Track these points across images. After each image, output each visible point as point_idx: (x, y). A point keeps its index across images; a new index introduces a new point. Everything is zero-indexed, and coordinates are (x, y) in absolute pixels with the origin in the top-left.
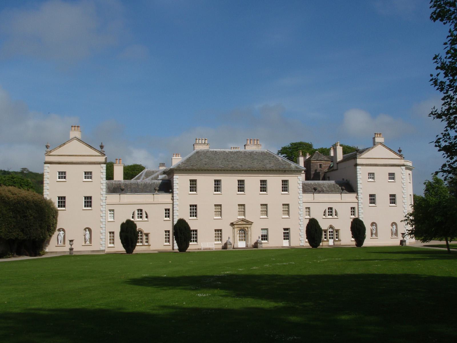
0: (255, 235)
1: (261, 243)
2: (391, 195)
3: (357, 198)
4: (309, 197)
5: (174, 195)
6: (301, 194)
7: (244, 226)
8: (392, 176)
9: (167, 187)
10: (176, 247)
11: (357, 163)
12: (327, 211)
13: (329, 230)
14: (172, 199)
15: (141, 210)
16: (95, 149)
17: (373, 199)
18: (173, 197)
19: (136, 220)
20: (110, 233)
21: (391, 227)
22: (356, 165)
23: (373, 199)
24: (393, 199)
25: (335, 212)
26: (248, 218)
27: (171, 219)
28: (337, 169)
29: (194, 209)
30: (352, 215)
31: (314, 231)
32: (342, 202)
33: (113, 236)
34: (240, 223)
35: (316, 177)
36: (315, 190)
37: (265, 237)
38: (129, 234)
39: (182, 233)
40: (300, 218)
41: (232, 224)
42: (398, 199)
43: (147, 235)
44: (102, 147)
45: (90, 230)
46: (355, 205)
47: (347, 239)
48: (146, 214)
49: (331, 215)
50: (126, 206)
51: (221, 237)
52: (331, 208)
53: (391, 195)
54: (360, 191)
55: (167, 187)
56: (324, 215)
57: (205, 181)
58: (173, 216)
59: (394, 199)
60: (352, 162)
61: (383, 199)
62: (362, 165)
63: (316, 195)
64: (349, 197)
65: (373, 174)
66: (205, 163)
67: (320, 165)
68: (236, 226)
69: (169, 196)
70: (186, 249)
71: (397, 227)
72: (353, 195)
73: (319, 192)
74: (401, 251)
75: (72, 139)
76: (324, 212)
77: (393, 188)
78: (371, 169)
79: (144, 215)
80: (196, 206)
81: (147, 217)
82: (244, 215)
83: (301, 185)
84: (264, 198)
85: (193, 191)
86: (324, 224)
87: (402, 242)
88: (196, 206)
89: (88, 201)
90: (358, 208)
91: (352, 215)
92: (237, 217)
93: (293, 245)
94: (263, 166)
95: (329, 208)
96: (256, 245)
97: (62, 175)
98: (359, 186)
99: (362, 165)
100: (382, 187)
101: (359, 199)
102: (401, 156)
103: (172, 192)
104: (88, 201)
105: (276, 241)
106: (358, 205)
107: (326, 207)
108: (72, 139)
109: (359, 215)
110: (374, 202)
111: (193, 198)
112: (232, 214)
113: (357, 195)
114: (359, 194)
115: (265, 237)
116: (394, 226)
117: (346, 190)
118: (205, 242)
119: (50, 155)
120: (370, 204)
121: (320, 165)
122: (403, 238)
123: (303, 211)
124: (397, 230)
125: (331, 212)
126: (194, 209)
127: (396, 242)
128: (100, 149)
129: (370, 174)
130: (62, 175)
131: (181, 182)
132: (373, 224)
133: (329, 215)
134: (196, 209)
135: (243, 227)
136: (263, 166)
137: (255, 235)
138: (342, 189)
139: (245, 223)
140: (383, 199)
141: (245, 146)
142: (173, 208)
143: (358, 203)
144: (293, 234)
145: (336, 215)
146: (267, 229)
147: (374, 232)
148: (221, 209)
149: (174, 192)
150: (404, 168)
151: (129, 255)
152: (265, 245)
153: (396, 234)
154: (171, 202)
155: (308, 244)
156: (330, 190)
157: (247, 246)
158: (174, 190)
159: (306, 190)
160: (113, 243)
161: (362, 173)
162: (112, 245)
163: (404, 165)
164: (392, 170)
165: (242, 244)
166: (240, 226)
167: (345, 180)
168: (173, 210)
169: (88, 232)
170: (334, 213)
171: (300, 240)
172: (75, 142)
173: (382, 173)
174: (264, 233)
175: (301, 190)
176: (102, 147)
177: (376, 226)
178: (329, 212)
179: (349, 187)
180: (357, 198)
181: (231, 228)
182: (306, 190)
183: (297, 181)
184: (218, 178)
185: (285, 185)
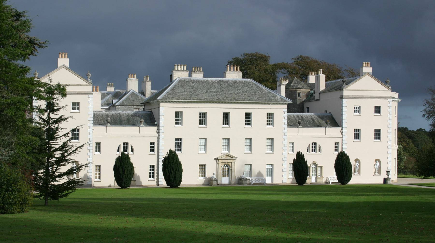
3: (342, 133)
4: (101, 129)
5: (160, 128)
6: (92, 127)
9: (151, 119)
10: (163, 182)
11: (344, 94)
12: (311, 146)
13: (312, 167)
14: (157, 132)
15: (127, 144)
17: (357, 134)
18: (158, 129)
21: (375, 163)
22: (342, 97)
23: (357, 134)
24: (378, 134)
25: (322, 147)
26: (231, 153)
28: (319, 100)
30: (335, 151)
32: (326, 136)
34: (224, 158)
35: (301, 108)
38: (123, 169)
39: (172, 167)
40: (89, 154)
41: (217, 159)
43: (321, 167)
45: (379, 161)
46: (339, 141)
47: (330, 176)
48: (132, 148)
49: (315, 151)
50: (114, 137)
51: (205, 173)
54: (345, 125)
55: (151, 119)
58: (158, 150)
59: (379, 135)
61: (367, 134)
62: (348, 97)
63: (301, 129)
64: (334, 131)
65: (78, 104)
66: (191, 93)
69: (155, 128)
70: (179, 184)
71: (380, 164)
74: (385, 188)
76: (119, 148)
77: (378, 122)
78: (357, 102)
80: (181, 139)
82: (228, 150)
83: (286, 118)
85: (178, 124)
87: (385, 180)
88: (181, 139)
90: (342, 142)
91: (335, 151)
92: (222, 152)
93: (275, 182)
94: (249, 98)
95: (124, 144)
97: (357, 109)
99: (348, 97)
100: (367, 122)
101: (344, 134)
103: (158, 125)
106: (342, 140)
107: (309, 142)
110: (358, 137)
113: (342, 129)
114: (344, 129)
117: (330, 124)
118: (190, 178)
119: (347, 90)
120: (354, 139)
122: (388, 175)
123: (288, 147)
124: (380, 168)
125: (315, 147)
126: (179, 141)
127: (379, 180)
129: (356, 108)
132: (356, 160)
133: (312, 151)
134: (181, 143)
136: (249, 98)
140: (367, 134)
142: (158, 141)
143: (342, 138)
146: (272, 165)
147: (357, 169)
149: (160, 125)
150: (390, 100)
153: (379, 172)
154: (157, 135)
155: (116, 184)
156: (314, 124)
157: (230, 182)
158: (160, 122)
159: (291, 123)
160: (99, 178)
161: (348, 105)
162: (98, 180)
165: (225, 181)
167: (328, 112)
168: (158, 144)
171: (285, 176)
172: (63, 70)
173: (368, 107)
175: (286, 123)
177: (359, 163)
178: (312, 147)
179: (333, 120)
180: (342, 133)
182: (291, 123)
183: (281, 113)
185: (203, 117)
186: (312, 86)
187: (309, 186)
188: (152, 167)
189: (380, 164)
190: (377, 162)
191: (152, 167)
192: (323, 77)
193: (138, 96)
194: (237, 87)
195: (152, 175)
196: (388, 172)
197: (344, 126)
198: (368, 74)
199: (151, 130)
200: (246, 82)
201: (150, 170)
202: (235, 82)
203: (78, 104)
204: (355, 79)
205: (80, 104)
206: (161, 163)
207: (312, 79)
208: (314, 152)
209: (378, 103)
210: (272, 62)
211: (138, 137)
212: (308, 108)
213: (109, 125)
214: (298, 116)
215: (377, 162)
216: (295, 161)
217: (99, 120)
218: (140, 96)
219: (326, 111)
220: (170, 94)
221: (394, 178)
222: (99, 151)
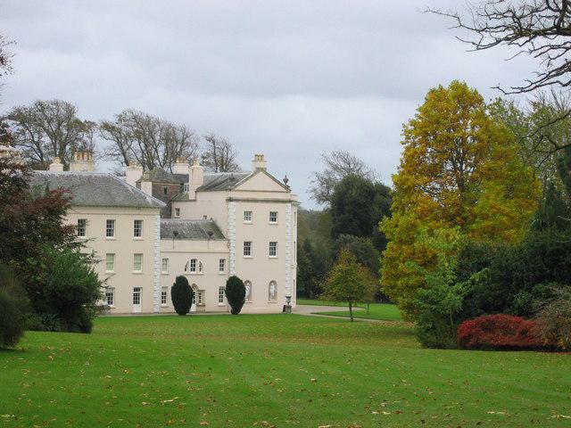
3: (229, 246)
17: (247, 248)
23: (247, 248)
61: (261, 248)
63: (177, 242)
67: (165, 190)
72: (224, 243)
73: (180, 238)
79: (197, 267)
107: (189, 258)
121: (165, 190)
124: (275, 292)
128: (283, 183)
144: (143, 296)
163: (290, 201)
167: (208, 218)
171: (156, 301)
176: (286, 181)
183: (152, 223)
189: (276, 288)
208: (193, 272)
212: (178, 210)
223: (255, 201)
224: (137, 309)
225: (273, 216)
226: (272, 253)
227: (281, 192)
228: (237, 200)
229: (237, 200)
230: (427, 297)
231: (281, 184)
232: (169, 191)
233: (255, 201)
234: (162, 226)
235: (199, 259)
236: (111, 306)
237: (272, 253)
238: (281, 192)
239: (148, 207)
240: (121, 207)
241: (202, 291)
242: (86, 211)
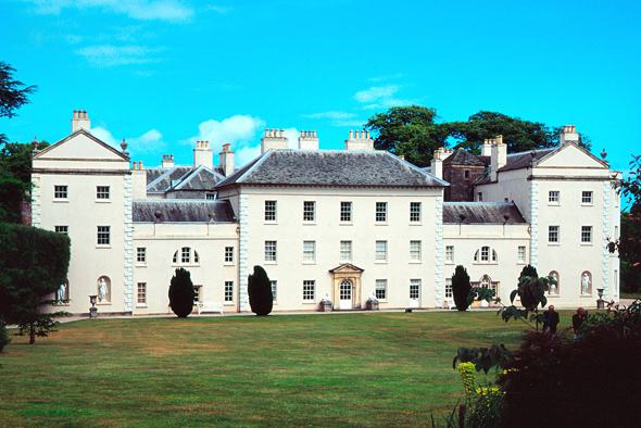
0: (365, 291)
1: (377, 304)
2: (551, 228)
3: (529, 232)
4: (146, 229)
7: (350, 275)
8: (587, 196)
9: (227, 213)
10: (246, 307)
12: (480, 252)
16: (595, 158)
17: (553, 234)
19: (186, 266)
20: (139, 284)
23: (553, 234)
27: (236, 264)
28: (496, 182)
29: (271, 248)
31: (461, 287)
33: (144, 290)
36: (467, 218)
37: (381, 293)
38: (183, 292)
41: (331, 272)
42: (561, 234)
44: (124, 146)
45: (107, 279)
46: (526, 244)
48: (196, 255)
50: (166, 241)
52: (487, 248)
53: (551, 228)
54: (534, 221)
55: (227, 213)
56: (175, 260)
57: (290, 204)
60: (524, 173)
61: (570, 233)
62: (43, 171)
63: (464, 227)
64: (518, 230)
65: (107, 188)
67: (467, 172)
68: (337, 275)
71: (590, 279)
72: (524, 227)
75: (77, 133)
77: (587, 216)
78: (61, 180)
79: (491, 256)
81: (196, 260)
82: (350, 258)
84: (381, 231)
86: (475, 276)
87: (600, 302)
89: (104, 235)
95: (483, 249)
96: (369, 305)
97: (61, 191)
98: (534, 212)
99: (43, 171)
101: (533, 234)
102: (604, 163)
104: (104, 235)
105: (398, 299)
107: (480, 245)
108: (77, 133)
109: (530, 260)
111: (270, 231)
112: (331, 257)
115: (381, 293)
116: (587, 278)
118: (287, 300)
124: (590, 285)
126: (271, 248)
127: (310, 307)
128: (601, 158)
130: (61, 191)
131: (250, 204)
134: (274, 248)
135: (347, 277)
137: (365, 291)
138: (506, 218)
139: (351, 270)
140: (570, 233)
141: (346, 141)
144: (423, 291)
145: (494, 259)
148: (350, 248)
151: (183, 324)
152: (385, 305)
154: (237, 237)
159: (448, 217)
161: (540, 190)
164: (103, 181)
165: (346, 305)
166: (343, 275)
167: (510, 200)
169: (104, 284)
170: (192, 257)
171: (437, 297)
172: (571, 147)
173: (571, 192)
174: (381, 287)
175: (131, 217)
176: (604, 155)
178: (183, 255)
179: (514, 214)
180: (529, 232)
181: (329, 278)
182: (448, 217)
183: (433, 204)
184: (416, 200)
186: (487, 161)
187: (282, 318)
188: (229, 284)
189: (590, 279)
190: (587, 278)
191: (229, 284)
192: (503, 148)
193: (212, 175)
194: (365, 163)
195: (229, 296)
196: (601, 291)
197: (533, 222)
198: (573, 142)
199: (227, 229)
200: (379, 156)
201: (227, 289)
202: (361, 157)
203: (107, 188)
204: (546, 153)
205: (110, 190)
206: (245, 282)
207: (487, 150)
208: (485, 262)
209: (103, 181)
210: (437, 121)
211: (207, 238)
212: (480, 194)
213: (212, 220)
214: (461, 207)
215: (587, 278)
216: (454, 279)
217: (142, 214)
218: (217, 175)
219: (506, 199)
220: (257, 175)
221: (617, 300)
222: (143, 259)
223: (563, 178)
224: (414, 303)
225: (587, 196)
226: (551, 240)
227: (115, 161)
228: (541, 178)
229: (541, 178)
230: (238, 351)
231: (599, 160)
232: (471, 174)
233: (563, 178)
234: (444, 207)
235: (492, 246)
236: (380, 300)
237: (551, 240)
238: (115, 161)
239: (426, 187)
240: (393, 187)
241: (496, 283)
242: (419, 193)
